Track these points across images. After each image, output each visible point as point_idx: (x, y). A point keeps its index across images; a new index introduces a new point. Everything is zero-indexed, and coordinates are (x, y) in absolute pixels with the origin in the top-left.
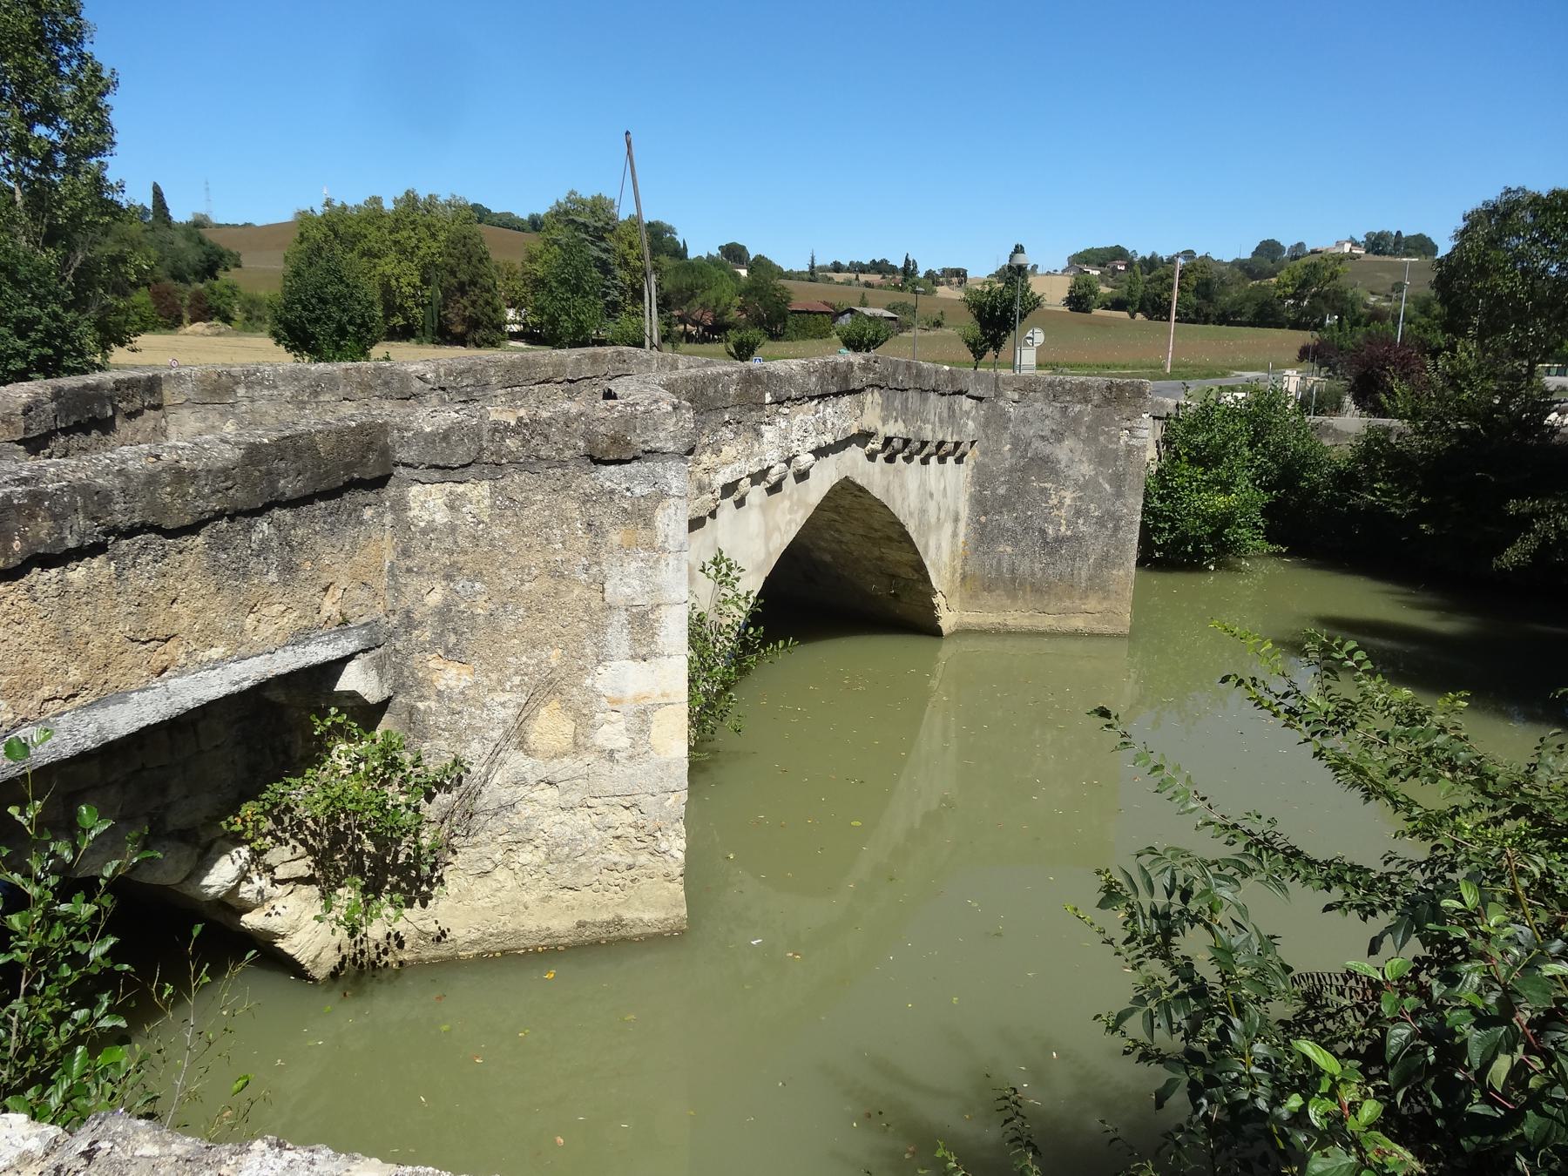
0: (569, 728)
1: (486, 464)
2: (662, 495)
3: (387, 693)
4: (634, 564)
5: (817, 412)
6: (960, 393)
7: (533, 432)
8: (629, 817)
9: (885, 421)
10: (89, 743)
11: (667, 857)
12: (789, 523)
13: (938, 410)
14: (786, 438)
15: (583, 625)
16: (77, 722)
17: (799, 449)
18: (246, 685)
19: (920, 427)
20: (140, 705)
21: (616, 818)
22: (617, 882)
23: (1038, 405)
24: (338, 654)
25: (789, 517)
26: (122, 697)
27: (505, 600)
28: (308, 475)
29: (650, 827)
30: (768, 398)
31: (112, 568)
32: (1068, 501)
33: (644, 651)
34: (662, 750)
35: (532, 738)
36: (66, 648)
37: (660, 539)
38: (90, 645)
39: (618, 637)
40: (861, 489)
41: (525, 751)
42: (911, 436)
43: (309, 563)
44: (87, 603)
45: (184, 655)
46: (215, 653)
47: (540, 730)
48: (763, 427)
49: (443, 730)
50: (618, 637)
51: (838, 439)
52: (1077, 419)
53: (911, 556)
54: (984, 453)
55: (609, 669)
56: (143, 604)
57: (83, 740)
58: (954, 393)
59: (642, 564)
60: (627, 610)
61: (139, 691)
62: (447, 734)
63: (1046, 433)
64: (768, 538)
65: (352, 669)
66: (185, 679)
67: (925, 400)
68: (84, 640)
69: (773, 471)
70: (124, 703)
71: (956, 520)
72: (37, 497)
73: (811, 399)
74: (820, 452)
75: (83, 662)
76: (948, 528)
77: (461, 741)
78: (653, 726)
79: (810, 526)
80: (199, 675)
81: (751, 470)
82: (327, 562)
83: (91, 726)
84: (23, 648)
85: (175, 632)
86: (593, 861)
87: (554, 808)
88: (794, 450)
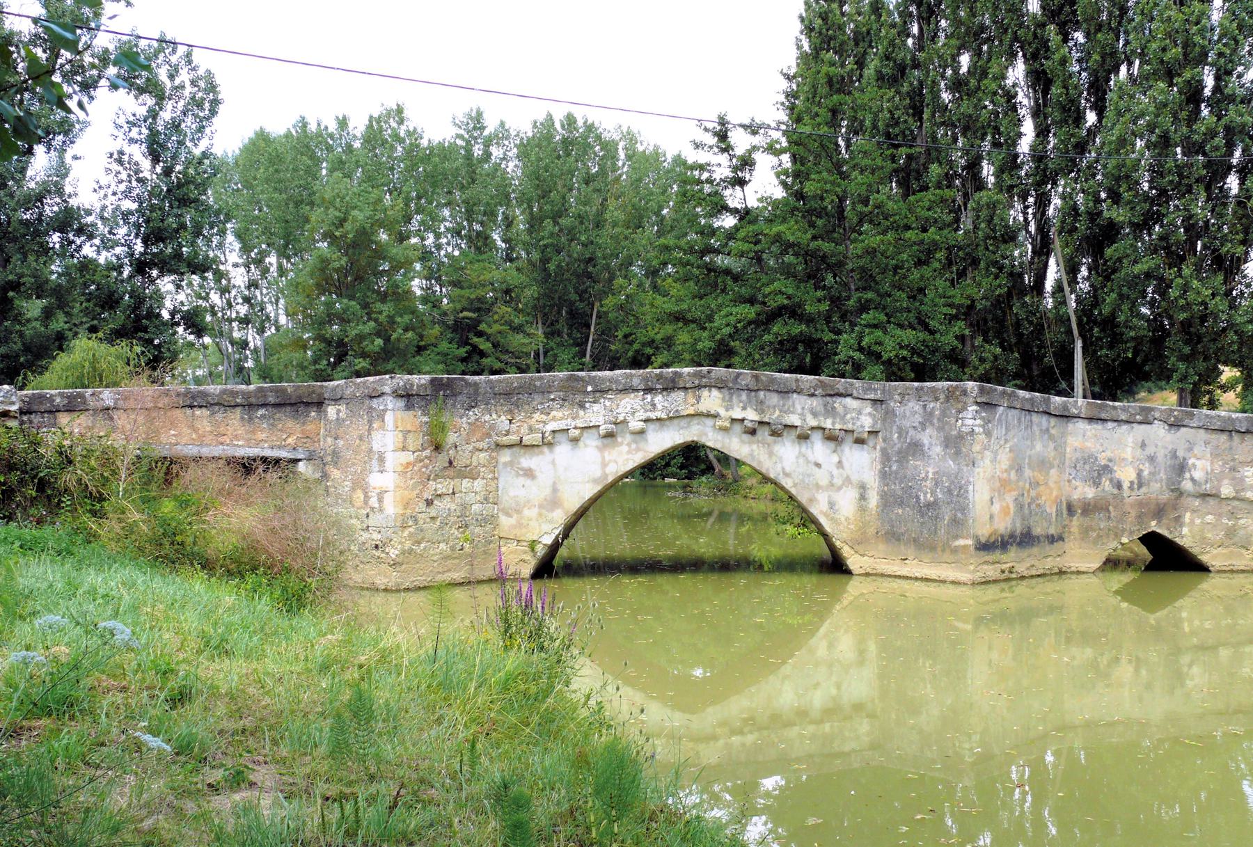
23: (910, 404)
25: (626, 456)
32: (930, 475)
46: (240, 443)
52: (931, 414)
56: (218, 425)
63: (916, 424)
65: (300, 463)
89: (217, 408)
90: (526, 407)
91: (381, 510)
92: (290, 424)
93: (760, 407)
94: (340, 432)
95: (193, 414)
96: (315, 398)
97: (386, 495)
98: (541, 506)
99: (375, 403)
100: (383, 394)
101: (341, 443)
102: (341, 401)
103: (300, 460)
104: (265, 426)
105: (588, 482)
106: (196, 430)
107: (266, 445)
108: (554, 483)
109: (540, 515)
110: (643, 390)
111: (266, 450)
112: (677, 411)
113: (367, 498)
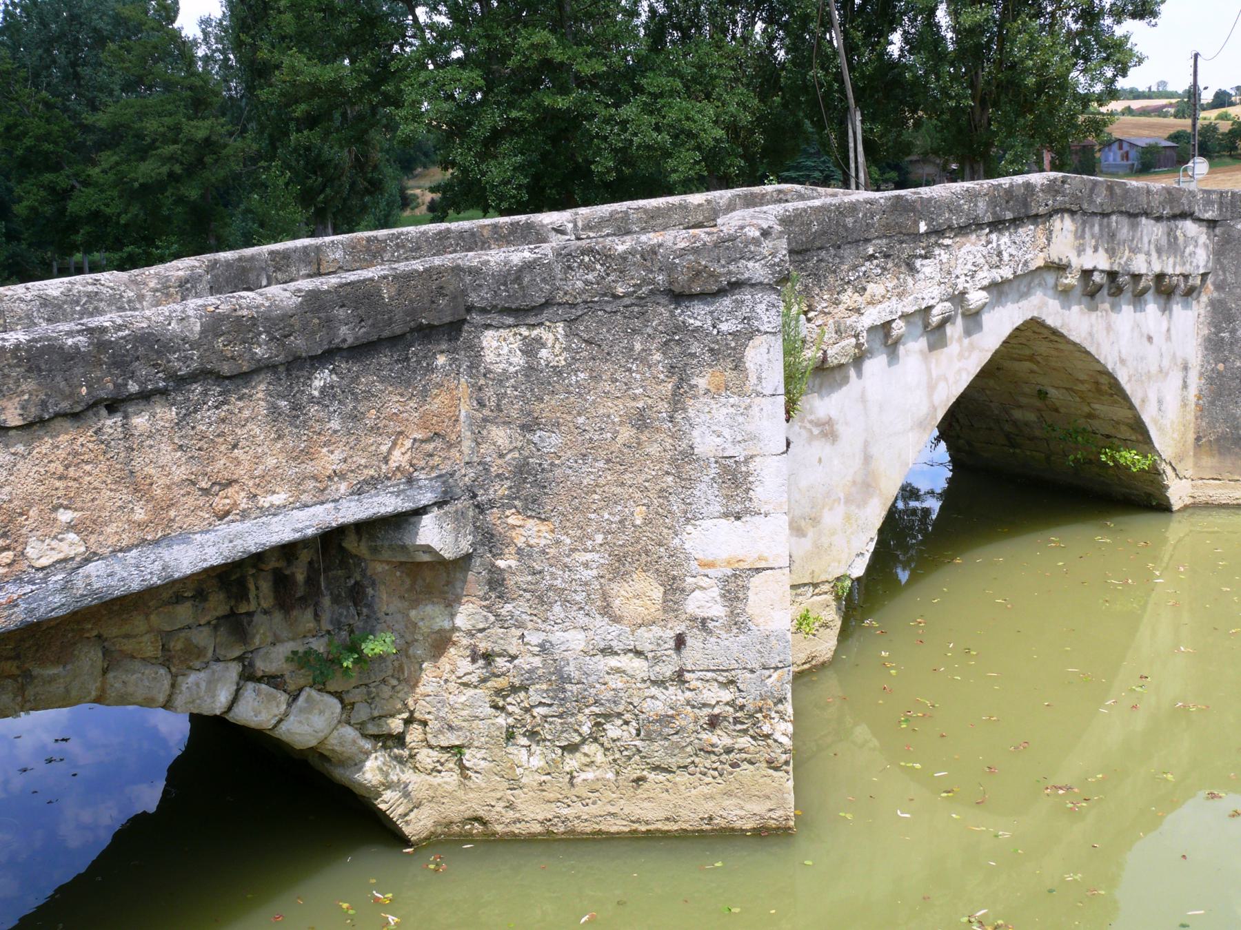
0: (658, 593)
1: (559, 304)
2: (752, 333)
3: (465, 546)
4: (724, 411)
5: (989, 242)
6: (1184, 216)
7: (608, 267)
8: (726, 695)
9: (1080, 251)
10: (155, 579)
11: (770, 742)
12: (959, 371)
13: (1154, 237)
14: (949, 273)
15: (670, 479)
16: (144, 559)
17: (966, 285)
18: (310, 532)
19: (1129, 259)
20: (202, 546)
21: (712, 695)
22: (715, 766)
24: (408, 506)
26: (185, 537)
27: (584, 451)
28: (370, 322)
29: (751, 707)
30: (923, 227)
31: (174, 413)
33: (738, 508)
34: (762, 620)
35: (617, 603)
36: (131, 488)
37: (753, 379)
38: (154, 486)
39: (706, 493)
40: (1055, 332)
41: (610, 616)
42: (1116, 268)
43: (373, 411)
44: (151, 447)
45: (245, 500)
46: (279, 499)
47: (625, 594)
48: (918, 263)
49: (525, 590)
50: (706, 493)
51: (1019, 272)
53: (1129, 414)
54: (1219, 287)
55: (699, 528)
57: (149, 576)
58: (1175, 217)
59: (732, 410)
60: (716, 462)
61: (202, 532)
62: (528, 595)
64: (931, 388)
65: (427, 520)
66: (248, 524)
67: (1134, 227)
68: (148, 481)
69: (934, 312)
70: (188, 543)
71: (1186, 368)
72: (102, 346)
73: (980, 226)
74: (997, 289)
75: (147, 501)
76: (1175, 379)
77: (542, 602)
78: (750, 593)
79: (989, 372)
80: (260, 520)
81: (905, 310)
82: (394, 411)
83: (156, 563)
84: (92, 486)
85: (235, 477)
86: (688, 740)
87: (644, 681)
88: (960, 287)
89: (198, 388)
90: (831, 279)
91: (737, 623)
92: (393, 403)
93: (1111, 243)
94: (547, 408)
95: (127, 434)
96: (444, 312)
97: (756, 581)
98: (848, 501)
99: (697, 315)
100: (736, 285)
101: (551, 441)
102: (546, 314)
103: (420, 512)
104: (335, 424)
105: (912, 429)
106: (139, 487)
107: (343, 487)
108: (866, 444)
109: (848, 518)
110: (989, 224)
111: (344, 503)
112: (1026, 264)
113: (674, 589)
